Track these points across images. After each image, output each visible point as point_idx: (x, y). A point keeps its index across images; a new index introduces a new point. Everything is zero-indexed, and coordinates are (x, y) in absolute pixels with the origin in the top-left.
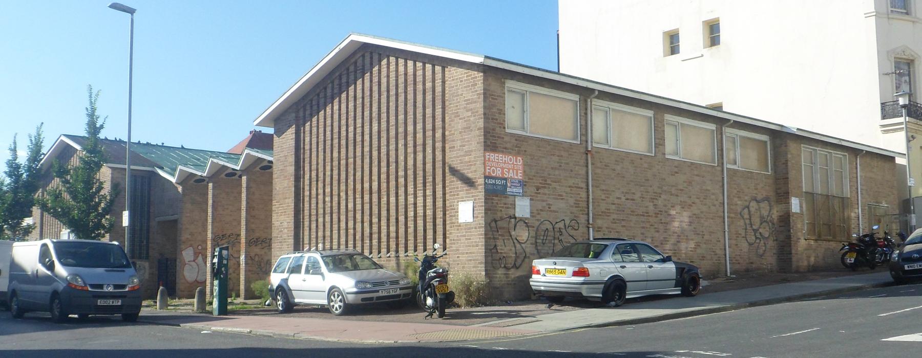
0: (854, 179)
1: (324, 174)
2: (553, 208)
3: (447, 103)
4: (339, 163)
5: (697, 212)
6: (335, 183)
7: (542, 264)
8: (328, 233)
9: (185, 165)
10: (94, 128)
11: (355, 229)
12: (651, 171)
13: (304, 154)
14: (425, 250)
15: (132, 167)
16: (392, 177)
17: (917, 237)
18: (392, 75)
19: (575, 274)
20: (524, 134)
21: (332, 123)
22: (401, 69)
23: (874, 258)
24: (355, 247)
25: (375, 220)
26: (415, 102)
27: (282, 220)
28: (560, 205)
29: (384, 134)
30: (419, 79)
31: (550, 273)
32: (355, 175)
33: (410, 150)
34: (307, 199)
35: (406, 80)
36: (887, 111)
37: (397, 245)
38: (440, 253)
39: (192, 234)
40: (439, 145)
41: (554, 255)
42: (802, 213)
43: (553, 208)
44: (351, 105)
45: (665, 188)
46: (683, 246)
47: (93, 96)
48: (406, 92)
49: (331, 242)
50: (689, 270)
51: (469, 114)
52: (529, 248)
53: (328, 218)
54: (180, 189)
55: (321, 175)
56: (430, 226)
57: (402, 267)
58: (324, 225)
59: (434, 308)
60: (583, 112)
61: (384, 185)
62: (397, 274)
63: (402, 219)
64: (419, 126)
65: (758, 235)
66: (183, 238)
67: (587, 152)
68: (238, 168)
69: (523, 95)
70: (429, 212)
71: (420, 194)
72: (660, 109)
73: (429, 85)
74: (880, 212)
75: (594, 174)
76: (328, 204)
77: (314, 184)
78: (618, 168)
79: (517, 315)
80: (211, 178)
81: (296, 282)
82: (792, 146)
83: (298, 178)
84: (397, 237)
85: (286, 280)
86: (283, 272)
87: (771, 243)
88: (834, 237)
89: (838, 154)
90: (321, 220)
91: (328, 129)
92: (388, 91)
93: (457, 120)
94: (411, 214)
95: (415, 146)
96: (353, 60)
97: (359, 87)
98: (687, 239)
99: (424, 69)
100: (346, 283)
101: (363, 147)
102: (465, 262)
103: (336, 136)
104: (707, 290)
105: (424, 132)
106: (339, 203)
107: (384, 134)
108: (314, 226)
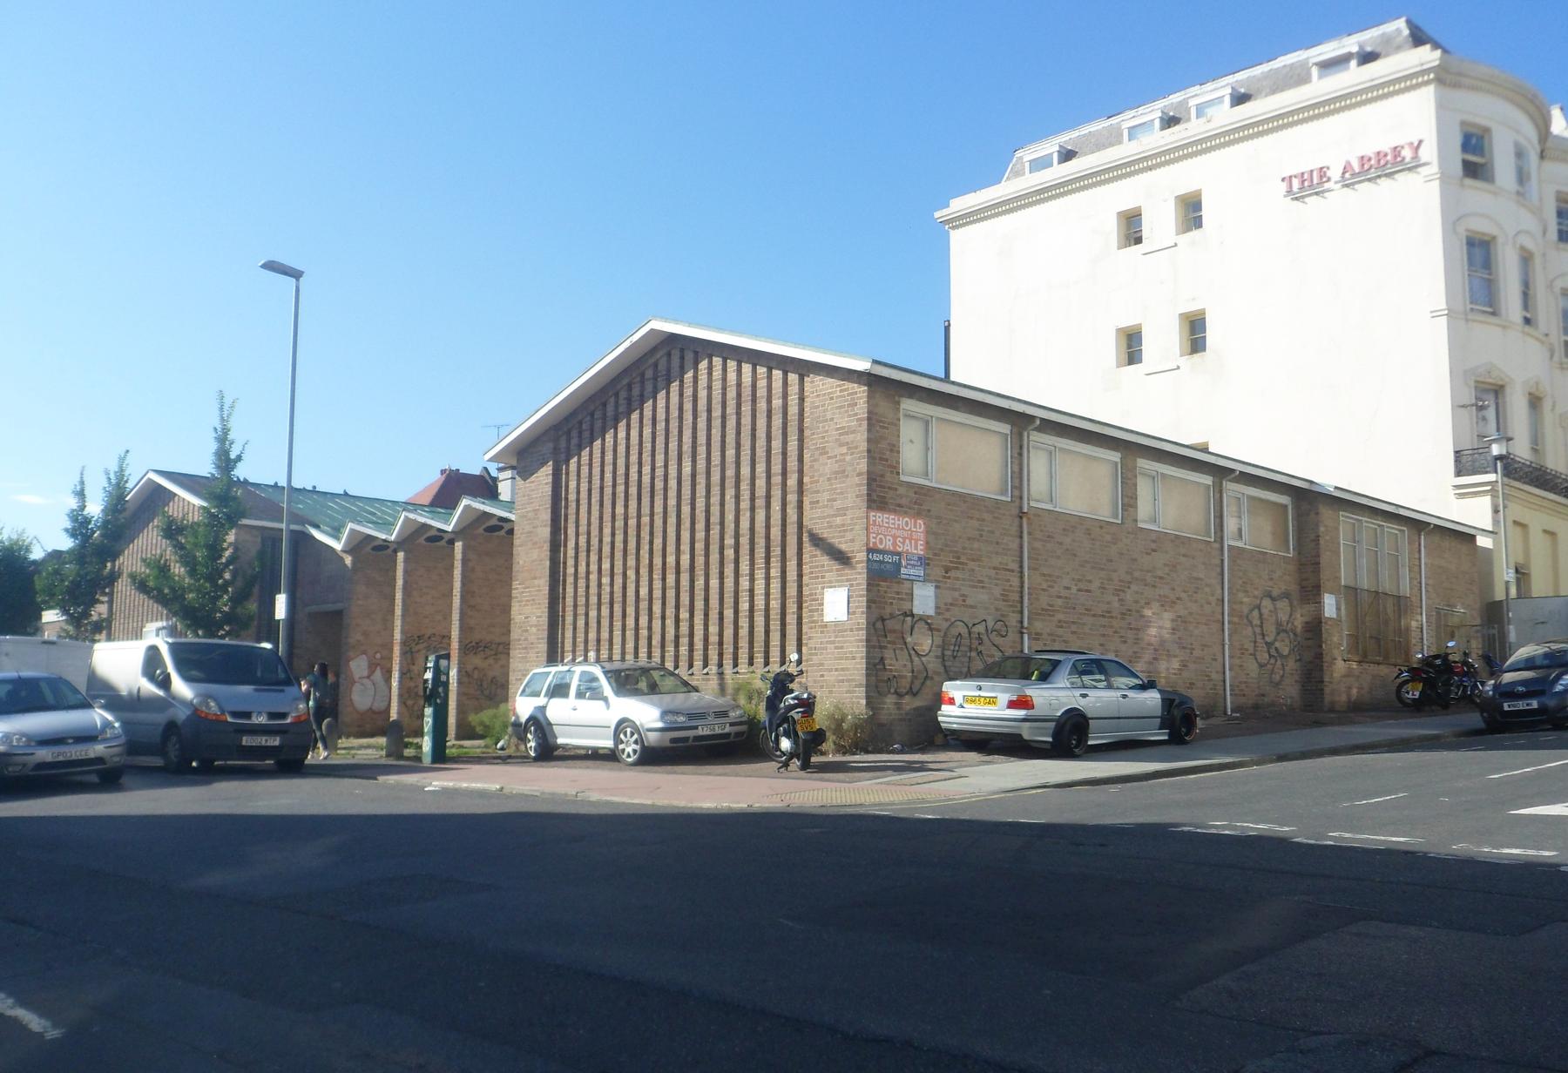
0: (1415, 568)
1: (601, 541)
2: (969, 602)
3: (807, 433)
4: (626, 524)
5: (1182, 613)
6: (619, 555)
7: (958, 688)
8: (605, 635)
9: (359, 523)
10: (225, 461)
11: (650, 628)
12: (1115, 545)
13: (566, 507)
14: (767, 663)
15: (293, 527)
16: (714, 548)
17: (1517, 662)
18: (717, 385)
19: (1012, 705)
20: (927, 483)
21: (615, 458)
22: (732, 376)
23: (1449, 692)
24: (650, 657)
25: (684, 615)
26: (754, 429)
27: (528, 612)
28: (979, 597)
29: (701, 480)
30: (762, 392)
31: (969, 703)
32: (651, 543)
33: (745, 504)
34: (570, 580)
35: (739, 395)
36: (1464, 463)
37: (721, 655)
38: (793, 669)
39: (365, 634)
40: (792, 498)
41: (967, 675)
42: (1338, 620)
43: (969, 602)
44: (647, 431)
45: (1137, 574)
46: (1162, 666)
47: (226, 407)
48: (739, 413)
49: (611, 649)
50: (1181, 703)
51: (844, 450)
52: (933, 664)
53: (605, 611)
54: (348, 560)
55: (595, 541)
56: (775, 626)
57: (730, 690)
58: (599, 622)
59: (792, 755)
60: (1016, 451)
61: (700, 560)
62: (721, 701)
63: (729, 613)
64: (761, 468)
65: (1273, 652)
66: (351, 641)
67: (1021, 515)
68: (450, 528)
69: (927, 423)
70: (775, 604)
71: (760, 574)
72: (1131, 449)
73: (777, 402)
74: (1455, 621)
75: (1031, 549)
76: (606, 589)
77: (583, 555)
78: (1068, 540)
79: (922, 767)
80: (402, 543)
81: (559, 711)
82: (1326, 513)
83: (556, 545)
84: (721, 643)
85: (543, 709)
86: (537, 694)
87: (1291, 664)
88: (1386, 657)
89: (1392, 528)
90: (593, 614)
91: (609, 469)
92: (709, 411)
93: (823, 459)
94: (744, 606)
95: (753, 499)
96: (652, 361)
97: (661, 403)
98: (1169, 656)
99: (769, 377)
100: (646, 714)
101: (666, 498)
102: (836, 681)
103: (621, 480)
104: (1207, 735)
105: (769, 477)
106: (624, 588)
107: (701, 480)
108: (581, 623)
